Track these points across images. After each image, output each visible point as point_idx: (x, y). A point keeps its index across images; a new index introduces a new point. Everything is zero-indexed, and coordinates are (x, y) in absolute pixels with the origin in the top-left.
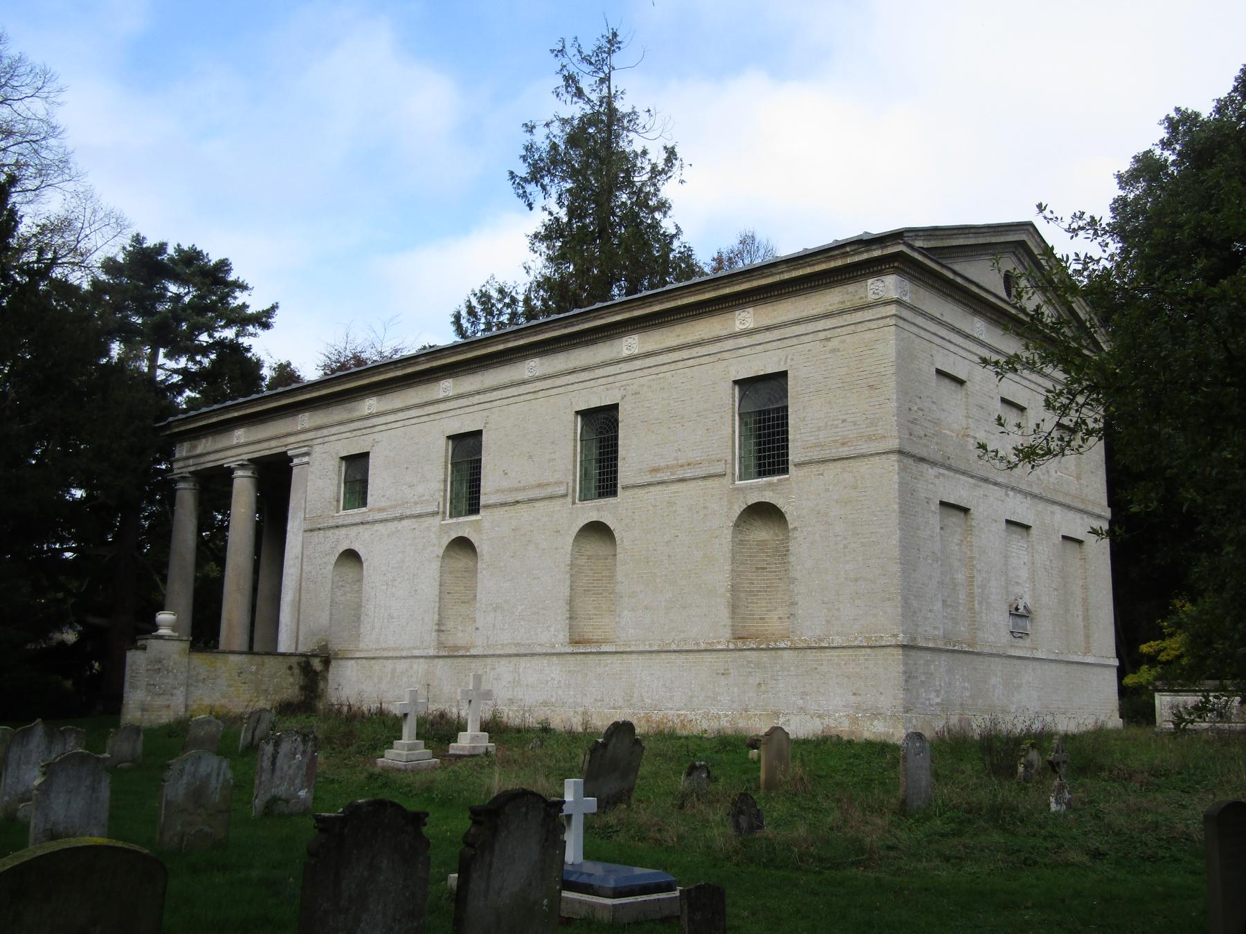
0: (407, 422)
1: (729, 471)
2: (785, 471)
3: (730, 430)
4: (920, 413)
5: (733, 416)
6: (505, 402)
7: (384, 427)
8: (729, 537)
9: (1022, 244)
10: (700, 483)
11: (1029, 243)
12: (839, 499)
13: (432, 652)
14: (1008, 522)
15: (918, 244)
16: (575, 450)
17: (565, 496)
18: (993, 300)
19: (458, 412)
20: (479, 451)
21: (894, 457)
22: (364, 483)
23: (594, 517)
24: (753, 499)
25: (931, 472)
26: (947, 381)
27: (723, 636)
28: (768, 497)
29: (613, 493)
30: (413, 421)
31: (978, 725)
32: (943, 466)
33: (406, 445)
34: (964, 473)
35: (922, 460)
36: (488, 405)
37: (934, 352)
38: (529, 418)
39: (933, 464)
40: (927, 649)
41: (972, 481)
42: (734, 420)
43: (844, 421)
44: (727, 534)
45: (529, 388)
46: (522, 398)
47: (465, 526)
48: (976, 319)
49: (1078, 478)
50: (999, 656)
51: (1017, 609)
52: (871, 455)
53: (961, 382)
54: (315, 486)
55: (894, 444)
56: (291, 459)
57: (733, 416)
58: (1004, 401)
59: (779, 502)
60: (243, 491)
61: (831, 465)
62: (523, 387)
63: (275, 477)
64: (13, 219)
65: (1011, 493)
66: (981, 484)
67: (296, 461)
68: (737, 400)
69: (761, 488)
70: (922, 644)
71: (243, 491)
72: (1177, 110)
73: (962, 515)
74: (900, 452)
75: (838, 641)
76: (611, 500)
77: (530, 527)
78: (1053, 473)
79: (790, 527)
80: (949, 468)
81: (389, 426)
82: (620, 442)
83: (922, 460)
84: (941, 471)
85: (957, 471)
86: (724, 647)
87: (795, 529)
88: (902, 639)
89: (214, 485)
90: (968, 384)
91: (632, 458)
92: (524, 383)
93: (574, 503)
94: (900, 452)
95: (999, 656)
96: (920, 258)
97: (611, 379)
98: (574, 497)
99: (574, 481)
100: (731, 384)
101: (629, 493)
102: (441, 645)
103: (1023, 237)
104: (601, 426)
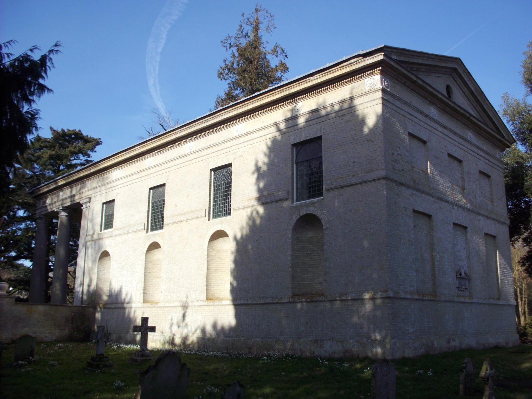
0: (131, 182)
1: (290, 197)
2: (321, 195)
3: (290, 173)
4: (400, 157)
5: (292, 165)
6: (176, 167)
7: (121, 186)
8: (290, 236)
9: (455, 70)
10: (274, 204)
11: (459, 70)
14: (454, 224)
15: (394, 57)
16: (210, 191)
18: (440, 96)
19: (155, 174)
21: (383, 182)
24: (303, 212)
25: (408, 192)
26: (415, 140)
28: (312, 210)
29: (229, 214)
30: (134, 181)
31: (439, 344)
32: (414, 189)
34: (427, 194)
35: (401, 184)
36: (168, 170)
37: (407, 122)
39: (408, 187)
40: (406, 299)
41: (433, 199)
42: (293, 167)
43: (354, 162)
44: (289, 233)
45: (188, 158)
46: (184, 164)
47: (156, 236)
48: (431, 108)
49: (492, 202)
50: (449, 301)
51: (461, 274)
52: (370, 181)
53: (424, 142)
55: (383, 173)
56: (82, 206)
57: (292, 165)
58: (449, 155)
59: (318, 213)
61: (348, 189)
62: (185, 158)
64: (28, 123)
65: (456, 208)
66: (437, 201)
67: (84, 206)
68: (294, 155)
69: (307, 206)
70: (403, 296)
73: (427, 219)
74: (387, 178)
76: (228, 218)
78: (478, 198)
79: (324, 227)
80: (418, 190)
81: (124, 185)
82: (232, 184)
83: (401, 184)
84: (414, 192)
85: (423, 192)
86: (287, 301)
87: (327, 228)
90: (428, 143)
92: (185, 156)
93: (209, 220)
94: (387, 178)
95: (449, 301)
96: (395, 65)
97: (228, 150)
98: (209, 216)
100: (290, 146)
103: (456, 66)
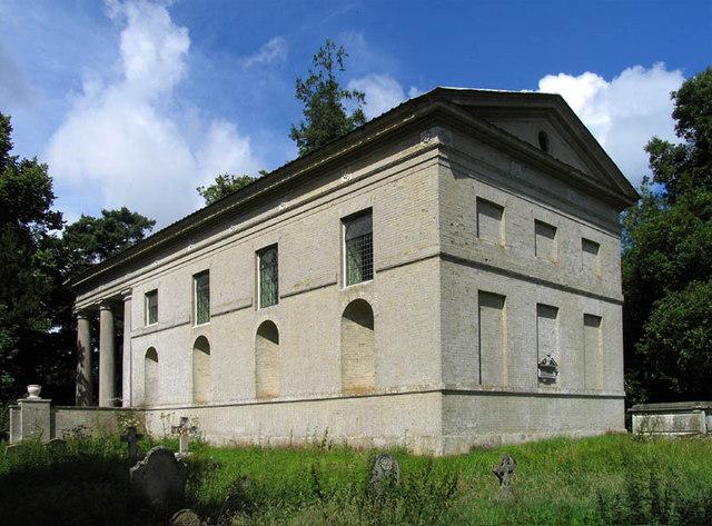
3: (339, 253)
9: (438, 111)
12: (410, 294)
13: (190, 405)
17: (251, 306)
20: (371, 226)
22: (156, 307)
23: (266, 318)
27: (251, 397)
28: (362, 295)
33: (170, 279)
38: (309, 231)
47: (364, 291)
54: (135, 309)
55: (437, 250)
60: (105, 317)
63: (117, 306)
71: (105, 317)
72: (104, 213)
74: (443, 256)
75: (404, 389)
77: (233, 333)
88: (442, 386)
89: (92, 314)
91: (216, 301)
99: (256, 296)
101: (284, 300)
102: (195, 401)
104: (269, 255)
